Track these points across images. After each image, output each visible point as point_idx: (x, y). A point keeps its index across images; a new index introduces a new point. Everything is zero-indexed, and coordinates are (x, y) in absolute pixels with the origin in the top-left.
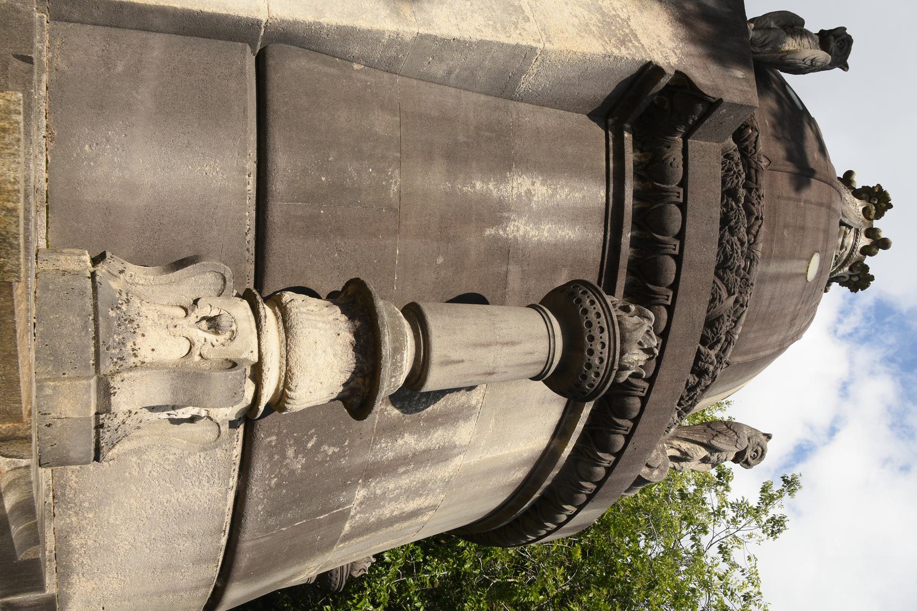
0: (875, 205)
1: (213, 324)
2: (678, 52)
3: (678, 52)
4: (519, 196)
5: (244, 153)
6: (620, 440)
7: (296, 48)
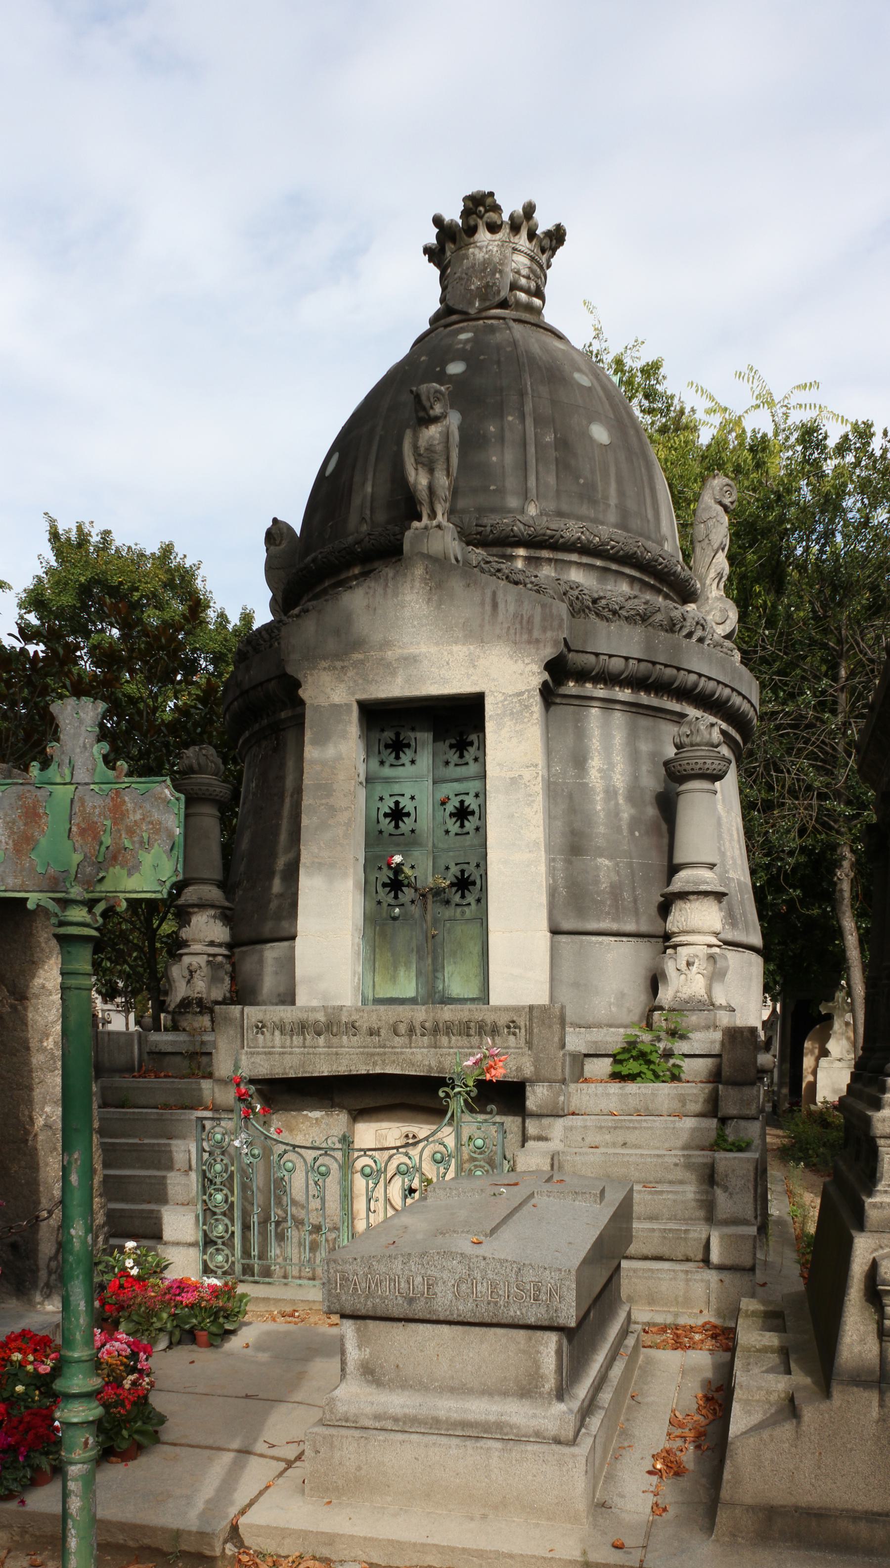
0: (486, 211)
1: (689, 964)
2: (526, 661)
3: (526, 661)
4: (601, 778)
5: (590, 943)
6: (693, 678)
7: (182, 811)
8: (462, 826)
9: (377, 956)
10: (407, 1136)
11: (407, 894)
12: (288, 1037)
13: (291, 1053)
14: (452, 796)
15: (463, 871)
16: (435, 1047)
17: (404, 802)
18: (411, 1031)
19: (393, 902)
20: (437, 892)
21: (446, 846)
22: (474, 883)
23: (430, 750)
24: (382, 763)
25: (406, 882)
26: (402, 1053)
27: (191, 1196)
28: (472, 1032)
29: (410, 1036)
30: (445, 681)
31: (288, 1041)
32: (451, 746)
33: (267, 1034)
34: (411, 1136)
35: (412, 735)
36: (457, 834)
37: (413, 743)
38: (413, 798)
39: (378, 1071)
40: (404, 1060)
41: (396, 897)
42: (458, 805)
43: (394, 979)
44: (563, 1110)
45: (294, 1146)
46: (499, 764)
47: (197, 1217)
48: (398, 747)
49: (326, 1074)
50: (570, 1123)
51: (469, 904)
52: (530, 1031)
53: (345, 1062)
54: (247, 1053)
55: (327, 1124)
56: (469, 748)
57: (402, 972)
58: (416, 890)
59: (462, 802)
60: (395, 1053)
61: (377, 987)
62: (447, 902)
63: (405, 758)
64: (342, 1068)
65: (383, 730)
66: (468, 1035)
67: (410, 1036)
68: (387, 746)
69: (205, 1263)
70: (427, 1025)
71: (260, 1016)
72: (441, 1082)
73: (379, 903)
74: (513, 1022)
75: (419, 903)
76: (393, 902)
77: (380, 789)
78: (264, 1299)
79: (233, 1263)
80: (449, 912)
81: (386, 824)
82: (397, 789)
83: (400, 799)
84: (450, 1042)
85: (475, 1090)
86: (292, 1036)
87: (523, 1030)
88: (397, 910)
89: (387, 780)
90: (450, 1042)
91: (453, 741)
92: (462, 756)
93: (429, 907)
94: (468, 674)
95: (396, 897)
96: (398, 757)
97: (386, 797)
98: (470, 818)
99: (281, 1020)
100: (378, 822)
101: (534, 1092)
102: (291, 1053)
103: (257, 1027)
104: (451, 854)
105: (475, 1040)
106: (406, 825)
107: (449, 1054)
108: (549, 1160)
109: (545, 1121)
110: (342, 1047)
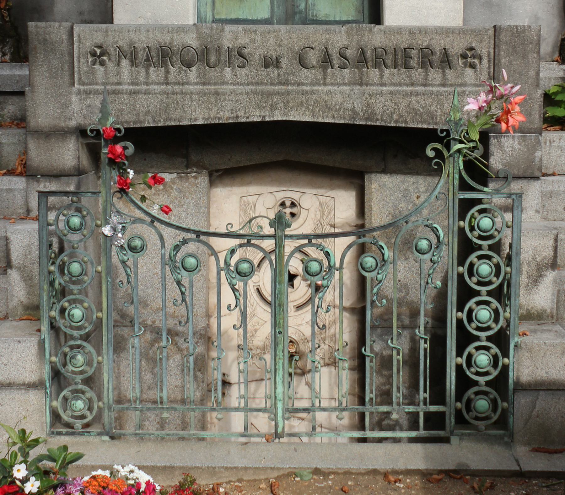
10: (283, 204)
12: (142, 70)
13: (147, 93)
16: (361, 84)
18: (325, 61)
26: (313, 92)
27: (11, 305)
28: (414, 63)
29: (325, 69)
31: (143, 74)
33: (111, 66)
34: (288, 203)
39: (278, 117)
40: (316, 102)
44: (540, 169)
45: (199, 234)
47: (41, 344)
49: (200, 122)
50: (550, 188)
52: (495, 63)
53: (228, 105)
54: (79, 92)
55: (180, 191)
60: (303, 93)
64: (225, 113)
66: (407, 67)
67: (325, 69)
69: (56, 417)
70: (349, 52)
71: (99, 38)
72: (430, 135)
74: (471, 49)
78: (165, 468)
79: (100, 410)
84: (381, 76)
85: (480, 146)
86: (147, 68)
87: (485, 61)
90: (381, 76)
99: (132, 44)
101: (500, 145)
102: (147, 93)
103: (94, 54)
105: (418, 74)
107: (381, 94)
108: (552, 242)
109: (516, 186)
110: (224, 83)
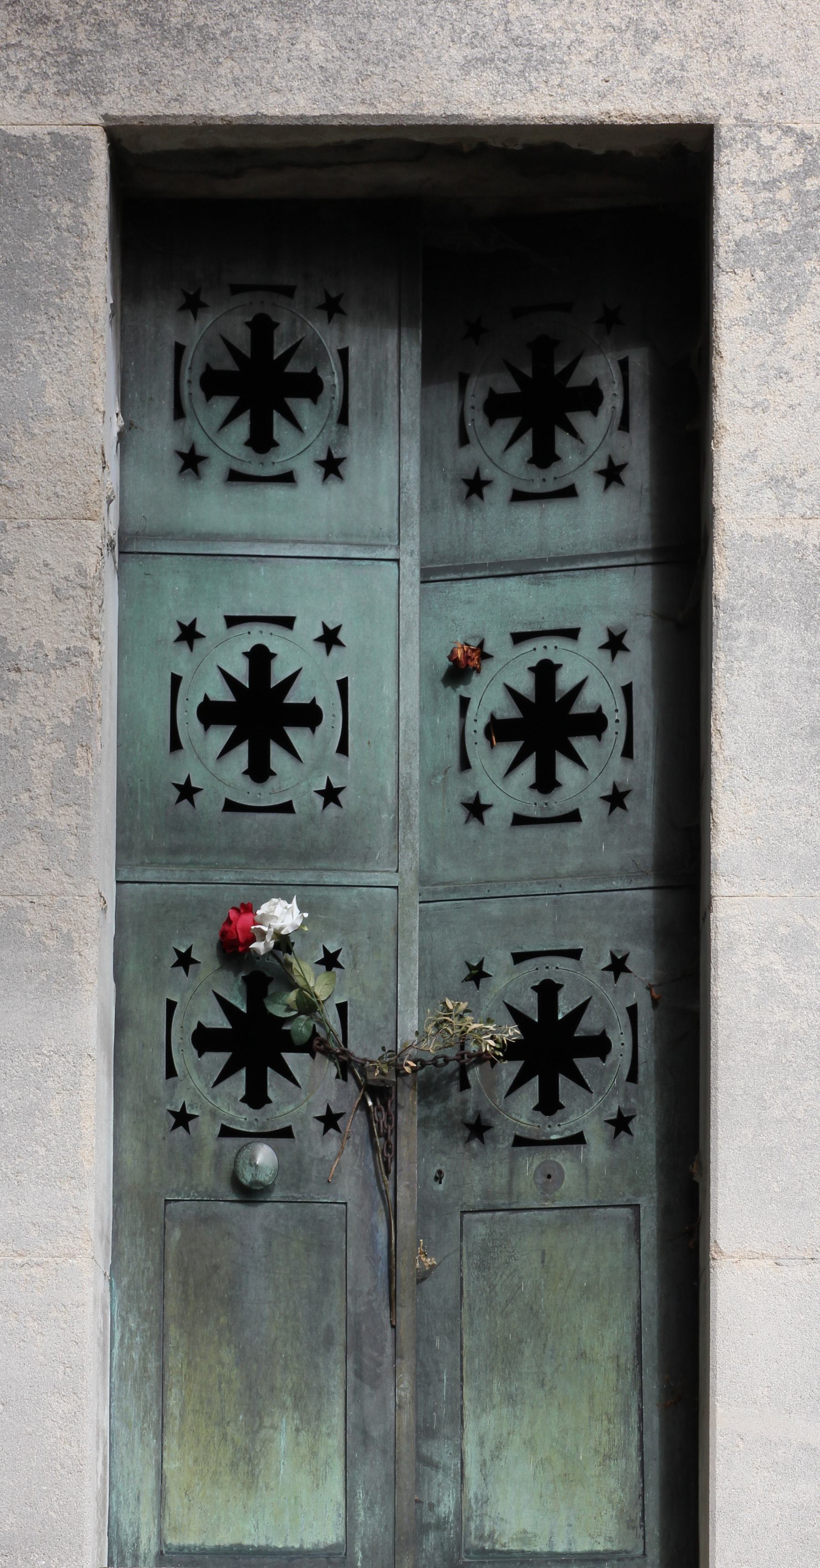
8: (546, 782)
9: (176, 1361)
11: (308, 1087)
14: (497, 643)
15: (548, 992)
17: (292, 654)
19: (243, 1117)
20: (448, 1073)
21: (471, 874)
22: (599, 1046)
23: (411, 416)
24: (191, 462)
25: (301, 1028)
30: (534, 58)
32: (496, 408)
35: (330, 337)
36: (519, 820)
37: (332, 378)
38: (330, 638)
41: (256, 1097)
42: (526, 685)
43: (248, 1465)
46: (775, 482)
48: (262, 389)
51: (578, 1139)
56: (581, 420)
57: (283, 1436)
58: (346, 1066)
59: (545, 672)
61: (174, 1500)
62: (478, 1129)
63: (298, 445)
65: (193, 305)
68: (213, 384)
73: (182, 1119)
75: (354, 1124)
76: (243, 1117)
77: (177, 595)
80: (480, 1172)
81: (214, 763)
82: (259, 595)
83: (273, 639)
88: (264, 1155)
89: (207, 552)
91: (506, 385)
92: (544, 456)
93: (408, 1146)
94: (635, 24)
95: (256, 1097)
96: (262, 441)
97: (211, 625)
98: (582, 745)
100: (176, 744)
104: (495, 909)
106: (297, 771)
